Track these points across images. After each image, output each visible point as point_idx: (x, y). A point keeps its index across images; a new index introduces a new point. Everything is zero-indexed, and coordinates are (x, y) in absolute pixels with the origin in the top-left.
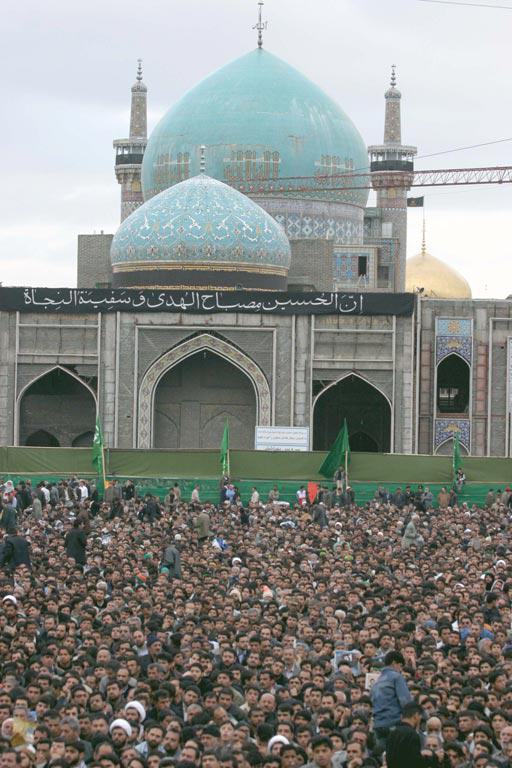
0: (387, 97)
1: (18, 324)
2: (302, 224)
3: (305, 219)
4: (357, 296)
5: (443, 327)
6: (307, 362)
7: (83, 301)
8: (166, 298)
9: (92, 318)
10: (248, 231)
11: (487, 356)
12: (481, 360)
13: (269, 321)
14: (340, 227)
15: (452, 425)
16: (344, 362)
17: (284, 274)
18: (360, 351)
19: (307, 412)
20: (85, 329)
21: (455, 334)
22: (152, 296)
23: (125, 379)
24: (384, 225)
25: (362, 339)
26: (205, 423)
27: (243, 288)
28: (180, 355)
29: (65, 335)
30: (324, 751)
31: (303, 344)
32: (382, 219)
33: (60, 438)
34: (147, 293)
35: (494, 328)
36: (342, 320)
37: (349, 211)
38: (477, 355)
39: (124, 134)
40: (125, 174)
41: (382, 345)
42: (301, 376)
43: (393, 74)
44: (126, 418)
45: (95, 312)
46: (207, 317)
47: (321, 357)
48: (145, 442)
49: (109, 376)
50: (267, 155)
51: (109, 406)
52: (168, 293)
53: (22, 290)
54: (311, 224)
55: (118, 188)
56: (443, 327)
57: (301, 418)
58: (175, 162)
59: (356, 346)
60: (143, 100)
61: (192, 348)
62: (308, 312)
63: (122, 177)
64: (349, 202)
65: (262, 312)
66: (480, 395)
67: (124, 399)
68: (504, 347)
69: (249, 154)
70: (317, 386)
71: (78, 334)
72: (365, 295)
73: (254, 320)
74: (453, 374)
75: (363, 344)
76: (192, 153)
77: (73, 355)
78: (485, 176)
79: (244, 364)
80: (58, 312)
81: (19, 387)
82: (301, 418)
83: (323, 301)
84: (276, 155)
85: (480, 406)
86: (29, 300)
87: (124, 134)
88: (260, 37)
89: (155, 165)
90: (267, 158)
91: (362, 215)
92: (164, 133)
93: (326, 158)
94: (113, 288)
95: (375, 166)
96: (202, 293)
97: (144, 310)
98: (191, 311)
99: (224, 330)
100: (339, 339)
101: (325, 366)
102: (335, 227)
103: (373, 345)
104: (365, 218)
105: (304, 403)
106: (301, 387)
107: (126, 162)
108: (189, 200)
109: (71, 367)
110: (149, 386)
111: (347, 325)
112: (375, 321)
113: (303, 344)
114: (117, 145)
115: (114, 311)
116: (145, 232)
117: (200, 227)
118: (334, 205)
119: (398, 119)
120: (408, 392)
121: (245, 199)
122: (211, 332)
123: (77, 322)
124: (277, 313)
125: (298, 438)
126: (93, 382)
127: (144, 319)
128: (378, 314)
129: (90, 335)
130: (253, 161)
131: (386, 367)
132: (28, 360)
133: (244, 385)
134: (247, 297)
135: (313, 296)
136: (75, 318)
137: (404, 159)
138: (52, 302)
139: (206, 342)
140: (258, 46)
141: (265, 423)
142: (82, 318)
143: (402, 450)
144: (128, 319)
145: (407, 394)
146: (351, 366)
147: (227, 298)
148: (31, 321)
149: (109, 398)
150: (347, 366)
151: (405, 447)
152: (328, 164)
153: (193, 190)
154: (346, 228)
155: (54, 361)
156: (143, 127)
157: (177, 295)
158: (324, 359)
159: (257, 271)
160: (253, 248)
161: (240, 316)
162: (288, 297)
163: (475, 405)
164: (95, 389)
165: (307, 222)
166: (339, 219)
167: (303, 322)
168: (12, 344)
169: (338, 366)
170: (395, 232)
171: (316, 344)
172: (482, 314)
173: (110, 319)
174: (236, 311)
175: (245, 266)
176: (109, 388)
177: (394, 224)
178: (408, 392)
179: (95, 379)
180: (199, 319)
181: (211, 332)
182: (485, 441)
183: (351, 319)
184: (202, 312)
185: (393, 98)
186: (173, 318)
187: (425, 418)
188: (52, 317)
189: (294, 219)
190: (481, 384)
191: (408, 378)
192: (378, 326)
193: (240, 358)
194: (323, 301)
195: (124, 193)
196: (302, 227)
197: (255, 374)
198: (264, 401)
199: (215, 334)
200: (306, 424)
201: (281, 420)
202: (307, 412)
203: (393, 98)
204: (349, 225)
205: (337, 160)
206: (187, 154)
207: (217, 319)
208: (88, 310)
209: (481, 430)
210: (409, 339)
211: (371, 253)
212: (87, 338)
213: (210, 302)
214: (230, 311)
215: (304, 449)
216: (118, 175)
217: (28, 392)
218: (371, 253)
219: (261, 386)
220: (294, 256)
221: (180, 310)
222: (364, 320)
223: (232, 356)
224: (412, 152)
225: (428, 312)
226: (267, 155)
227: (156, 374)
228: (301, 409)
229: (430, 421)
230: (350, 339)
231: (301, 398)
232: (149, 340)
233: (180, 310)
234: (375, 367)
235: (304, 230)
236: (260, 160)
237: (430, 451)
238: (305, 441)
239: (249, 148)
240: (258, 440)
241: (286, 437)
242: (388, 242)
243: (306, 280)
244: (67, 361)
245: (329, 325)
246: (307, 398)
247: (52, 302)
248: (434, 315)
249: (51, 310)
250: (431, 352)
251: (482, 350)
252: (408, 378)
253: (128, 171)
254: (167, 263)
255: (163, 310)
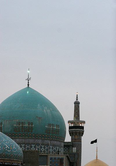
0: (74, 104)
2: (41, 147)
3: (32, 145)
10: (7, 148)
14: (54, 148)
24: (73, 148)
32: (73, 146)
37: (58, 143)
39: (72, 118)
40: (72, 133)
43: (77, 97)
50: (29, 123)
54: (44, 148)
58: (15, 125)
64: (61, 140)
69: (23, 123)
76: (3, 123)
84: (32, 124)
88: (28, 83)
90: (29, 125)
91: (63, 144)
93: (50, 125)
102: (52, 148)
104: (64, 146)
117: (9, 148)
118: (52, 141)
119: (79, 111)
130: (24, 125)
140: (28, 86)
152: (50, 126)
154: (57, 149)
165: (51, 147)
166: (54, 146)
177: (77, 148)
185: (77, 104)
189: (55, 147)
196: (41, 149)
203: (77, 104)
204: (58, 148)
205: (53, 125)
224: (84, 122)
226: (29, 123)
235: (50, 150)
236: (27, 125)
242: (74, 154)
253: (77, 132)
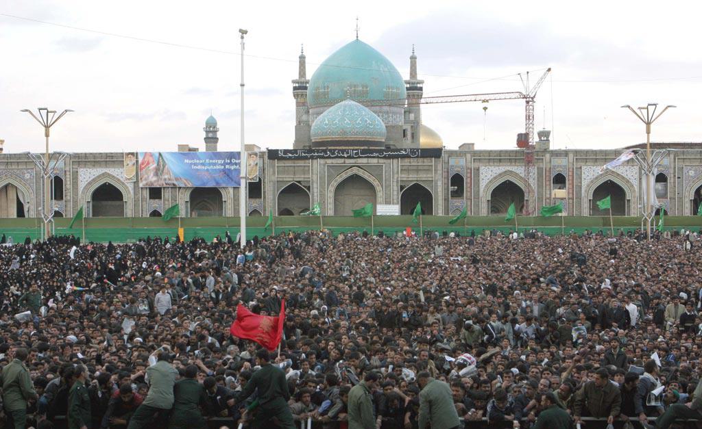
1: (276, 165)
4: (418, 150)
5: (452, 161)
6: (398, 178)
7: (303, 155)
8: (338, 152)
9: (307, 161)
11: (471, 173)
12: (469, 175)
13: (381, 161)
14: (394, 117)
15: (457, 202)
16: (413, 178)
17: (383, 140)
18: (420, 172)
19: (398, 198)
20: (304, 166)
21: (458, 165)
22: (332, 152)
23: (322, 186)
24: (411, 115)
25: (420, 168)
26: (354, 201)
27: (368, 147)
28: (344, 176)
29: (296, 168)
30: (548, 374)
31: (396, 170)
32: (410, 112)
33: (293, 211)
34: (330, 151)
35: (474, 162)
36: (412, 160)
38: (467, 173)
39: (296, 77)
41: (429, 170)
42: (395, 184)
44: (322, 204)
45: (309, 159)
46: (356, 160)
47: (403, 176)
48: (331, 212)
49: (315, 185)
51: (315, 198)
52: (339, 150)
53: (278, 150)
55: (295, 100)
56: (452, 161)
57: (395, 201)
59: (417, 171)
60: (304, 62)
61: (350, 173)
62: (397, 157)
63: (296, 96)
65: (378, 157)
66: (469, 190)
67: (322, 195)
68: (478, 169)
69: (355, 86)
70: (402, 188)
71: (302, 168)
72: (421, 149)
73: (375, 161)
74: (457, 180)
75: (420, 170)
76: (330, 86)
77: (299, 177)
78: (469, 98)
79: (371, 179)
80: (292, 159)
81: (278, 191)
82: (395, 201)
83: (404, 152)
85: (469, 194)
86: (281, 154)
87: (296, 77)
89: (314, 91)
92: (318, 75)
93: (388, 87)
94: (311, 148)
95: (408, 89)
96: (353, 150)
97: (329, 157)
98: (349, 157)
99: (361, 165)
100: (410, 168)
101: (405, 179)
103: (424, 170)
105: (396, 194)
106: (395, 188)
107: (298, 89)
108: (344, 110)
109: (299, 182)
110: (332, 189)
111: (414, 162)
112: (425, 160)
113: (396, 170)
114: (294, 82)
115: (317, 158)
116: (326, 125)
120: (440, 189)
121: (367, 109)
122: (357, 166)
123: (301, 163)
124: (385, 157)
125: (394, 210)
126: (309, 188)
127: (329, 161)
128: (427, 157)
129: (307, 168)
131: (431, 179)
132: (281, 180)
133: (371, 187)
134: (372, 152)
135: (399, 150)
136: (300, 161)
137: (419, 85)
138: (290, 155)
139: (355, 171)
141: (381, 203)
142: (303, 161)
143: (438, 213)
144: (322, 161)
145: (439, 190)
146: (416, 179)
147: (364, 152)
148: (282, 164)
149: (315, 194)
150: (414, 179)
151: (439, 212)
153: (345, 106)
155: (291, 179)
156: (305, 74)
157: (343, 151)
158: (404, 176)
159: (373, 140)
160: (371, 131)
161: (370, 159)
162: (389, 151)
163: (467, 194)
164: (309, 190)
166: (394, 113)
167: (395, 161)
168: (274, 173)
169: (410, 179)
170: (415, 118)
171: (401, 170)
172: (469, 156)
173: (315, 161)
174: (368, 157)
175: (369, 138)
176: (315, 190)
178: (440, 189)
179: (309, 187)
180: (352, 161)
181: (357, 166)
182: (471, 209)
183: (415, 160)
184: (353, 158)
186: (341, 161)
187: (446, 200)
188: (290, 162)
190: (469, 185)
191: (440, 183)
192: (427, 162)
193: (346, 174)
194: (404, 152)
195: (297, 103)
197: (375, 183)
198: (380, 194)
199: (359, 167)
200: (398, 204)
201: (388, 202)
202: (398, 198)
205: (393, 88)
206: (328, 87)
207: (360, 161)
208: (306, 158)
209: (469, 204)
210: (440, 167)
211: (408, 127)
212: (305, 170)
213: (357, 154)
214: (365, 157)
215: (397, 214)
216: (294, 96)
217: (282, 192)
218: (408, 127)
219: (378, 188)
220: (388, 132)
221: (344, 157)
222: (421, 160)
223: (366, 176)
224: (422, 82)
225: (446, 156)
227: (335, 184)
228: (395, 197)
229: (448, 201)
230: (415, 168)
231: (395, 193)
232: (331, 170)
233: (344, 157)
234: (426, 179)
237: (448, 214)
238: (397, 211)
239: (355, 83)
240: (377, 211)
241: (389, 209)
243: (391, 143)
244: (298, 180)
245: (406, 162)
246: (398, 193)
247: (290, 155)
248: (449, 157)
249: (290, 158)
250: (448, 172)
251: (469, 171)
252: (440, 183)
254: (336, 137)
255: (337, 157)
